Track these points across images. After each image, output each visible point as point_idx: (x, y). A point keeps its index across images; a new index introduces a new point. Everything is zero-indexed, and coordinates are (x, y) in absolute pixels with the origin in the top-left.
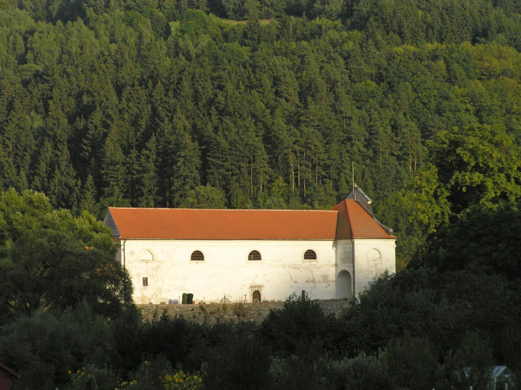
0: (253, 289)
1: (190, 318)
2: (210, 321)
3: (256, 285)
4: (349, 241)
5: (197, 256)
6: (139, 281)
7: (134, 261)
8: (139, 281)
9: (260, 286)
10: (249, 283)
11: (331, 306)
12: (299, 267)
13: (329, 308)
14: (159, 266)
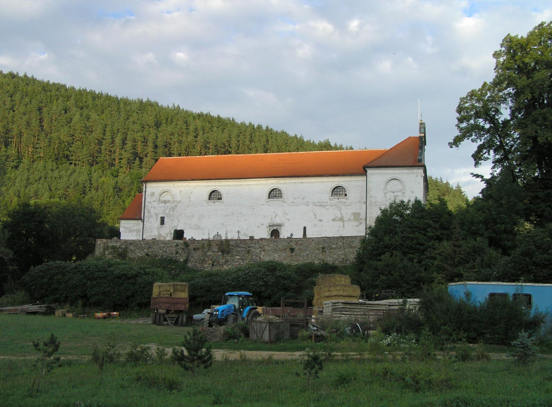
0: (271, 228)
1: (172, 254)
2: (192, 257)
3: (275, 224)
4: (364, 178)
5: (214, 196)
6: (157, 220)
7: (154, 201)
8: (157, 220)
9: (280, 225)
10: (267, 222)
11: (337, 244)
12: (325, 204)
13: (334, 246)
14: (176, 206)
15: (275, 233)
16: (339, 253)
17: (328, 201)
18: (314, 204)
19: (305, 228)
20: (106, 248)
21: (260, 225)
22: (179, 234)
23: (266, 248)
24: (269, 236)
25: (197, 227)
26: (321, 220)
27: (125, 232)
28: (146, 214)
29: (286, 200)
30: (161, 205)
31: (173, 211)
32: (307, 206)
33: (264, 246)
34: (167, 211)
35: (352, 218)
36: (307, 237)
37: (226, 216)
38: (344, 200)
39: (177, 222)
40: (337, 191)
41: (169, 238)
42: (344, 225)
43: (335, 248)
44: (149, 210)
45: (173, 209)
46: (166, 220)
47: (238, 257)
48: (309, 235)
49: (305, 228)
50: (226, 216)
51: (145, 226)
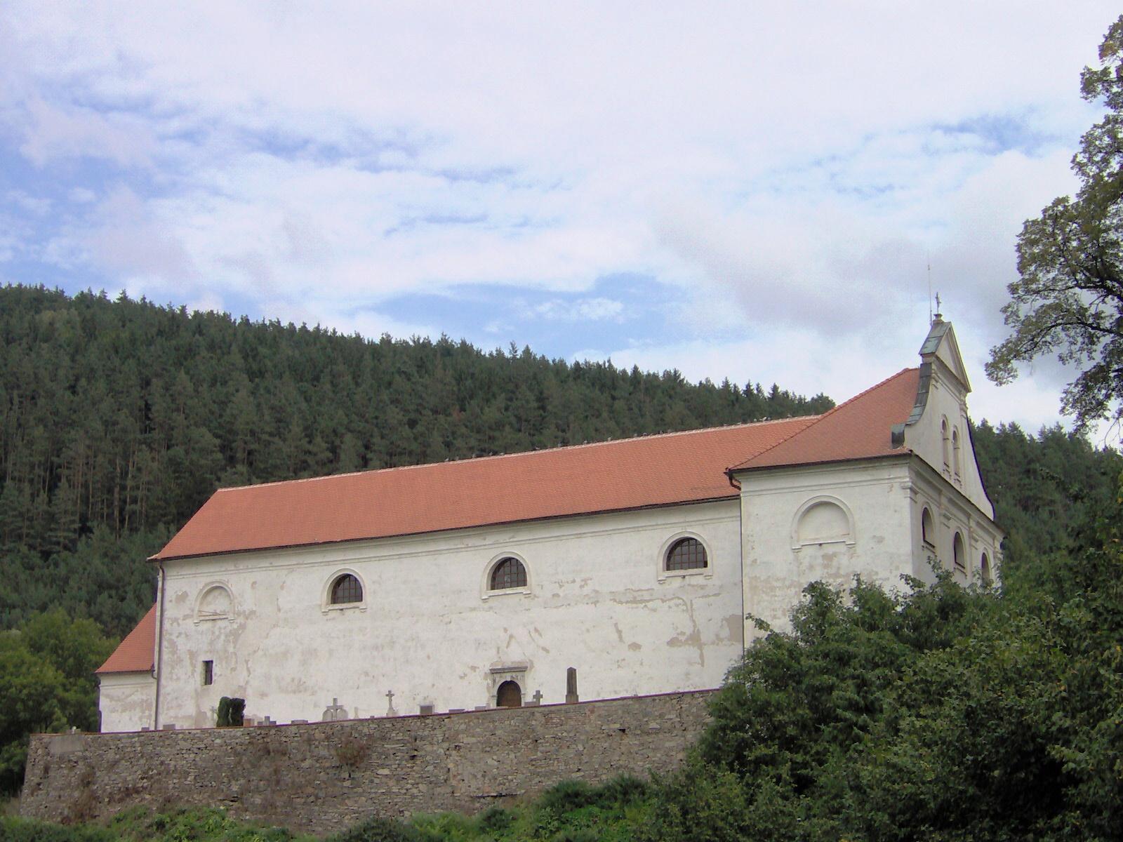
0: (497, 677)
3: (508, 664)
6: (193, 671)
8: (193, 671)
9: (522, 669)
11: (661, 716)
13: (653, 725)
15: (508, 692)
16: (668, 744)
17: (656, 586)
18: (615, 598)
19: (572, 674)
20: (746, 732)
21: (468, 671)
22: (232, 711)
23: (465, 739)
24: (493, 705)
25: (299, 687)
26: (635, 647)
27: (113, 711)
28: (165, 657)
29: (537, 591)
30: (206, 626)
31: (235, 642)
32: (595, 603)
33: (457, 732)
34: (220, 644)
35: (725, 633)
36: (580, 700)
37: (376, 648)
38: (699, 580)
39: (245, 673)
40: (684, 554)
41: (211, 720)
42: (702, 656)
43: (657, 732)
44: (173, 644)
45: (235, 635)
46: (216, 669)
47: (386, 772)
48: (585, 693)
49: (572, 674)
50: (376, 648)
51: (162, 691)
